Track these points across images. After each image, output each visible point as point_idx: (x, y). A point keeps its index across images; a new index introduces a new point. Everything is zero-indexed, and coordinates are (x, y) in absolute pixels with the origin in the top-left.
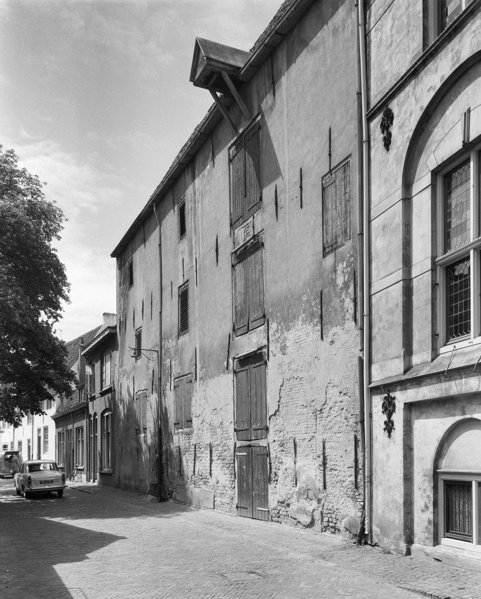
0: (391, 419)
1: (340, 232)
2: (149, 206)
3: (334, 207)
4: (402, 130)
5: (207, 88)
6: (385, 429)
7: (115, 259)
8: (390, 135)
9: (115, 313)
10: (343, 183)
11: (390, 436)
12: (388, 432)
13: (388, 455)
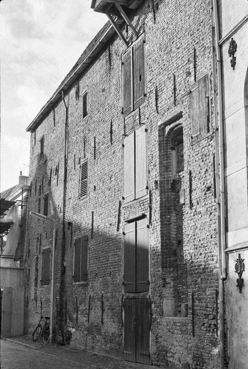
0: (242, 278)
1: (203, 126)
2: (41, 114)
3: (198, 107)
4: (242, 57)
5: (104, 12)
6: (237, 286)
7: (29, 133)
8: (234, 59)
9: (135, 222)
10: (204, 90)
11: (241, 292)
12: (240, 288)
13: (240, 308)
